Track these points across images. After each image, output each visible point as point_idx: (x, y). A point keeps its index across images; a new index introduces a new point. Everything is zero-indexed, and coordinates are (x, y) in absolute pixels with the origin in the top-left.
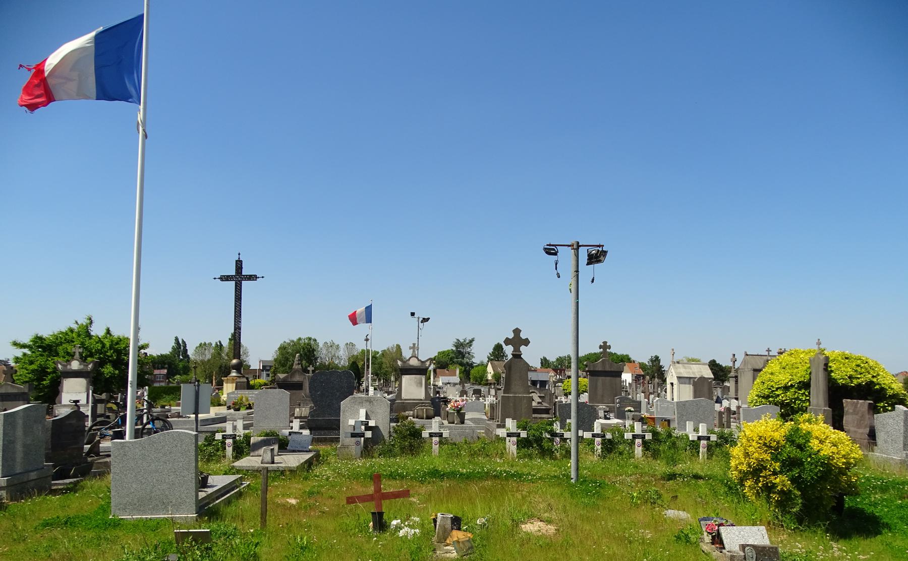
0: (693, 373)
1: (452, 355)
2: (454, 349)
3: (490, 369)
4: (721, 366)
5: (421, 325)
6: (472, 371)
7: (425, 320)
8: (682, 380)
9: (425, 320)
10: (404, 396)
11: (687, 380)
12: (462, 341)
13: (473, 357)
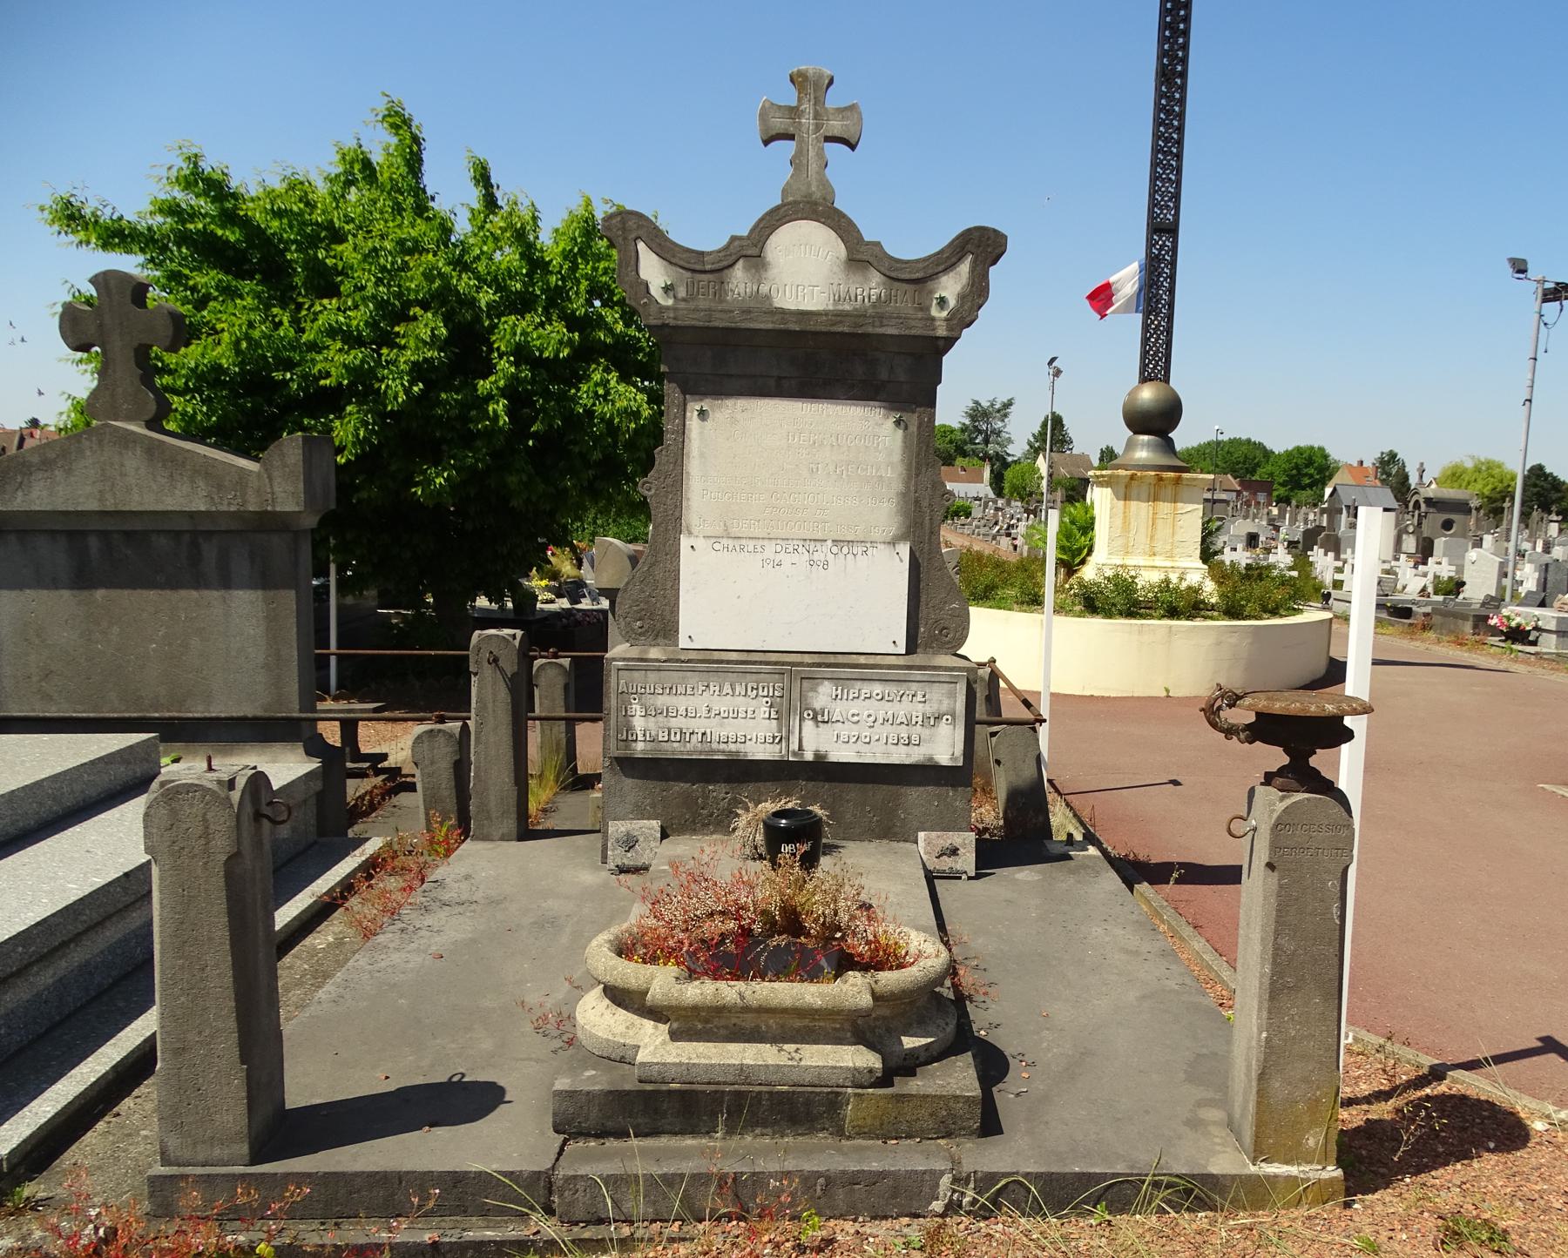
1: (959, 436)
2: (967, 422)
3: (1042, 464)
4: (1555, 478)
6: (1008, 474)
12: (985, 404)
13: (1010, 441)
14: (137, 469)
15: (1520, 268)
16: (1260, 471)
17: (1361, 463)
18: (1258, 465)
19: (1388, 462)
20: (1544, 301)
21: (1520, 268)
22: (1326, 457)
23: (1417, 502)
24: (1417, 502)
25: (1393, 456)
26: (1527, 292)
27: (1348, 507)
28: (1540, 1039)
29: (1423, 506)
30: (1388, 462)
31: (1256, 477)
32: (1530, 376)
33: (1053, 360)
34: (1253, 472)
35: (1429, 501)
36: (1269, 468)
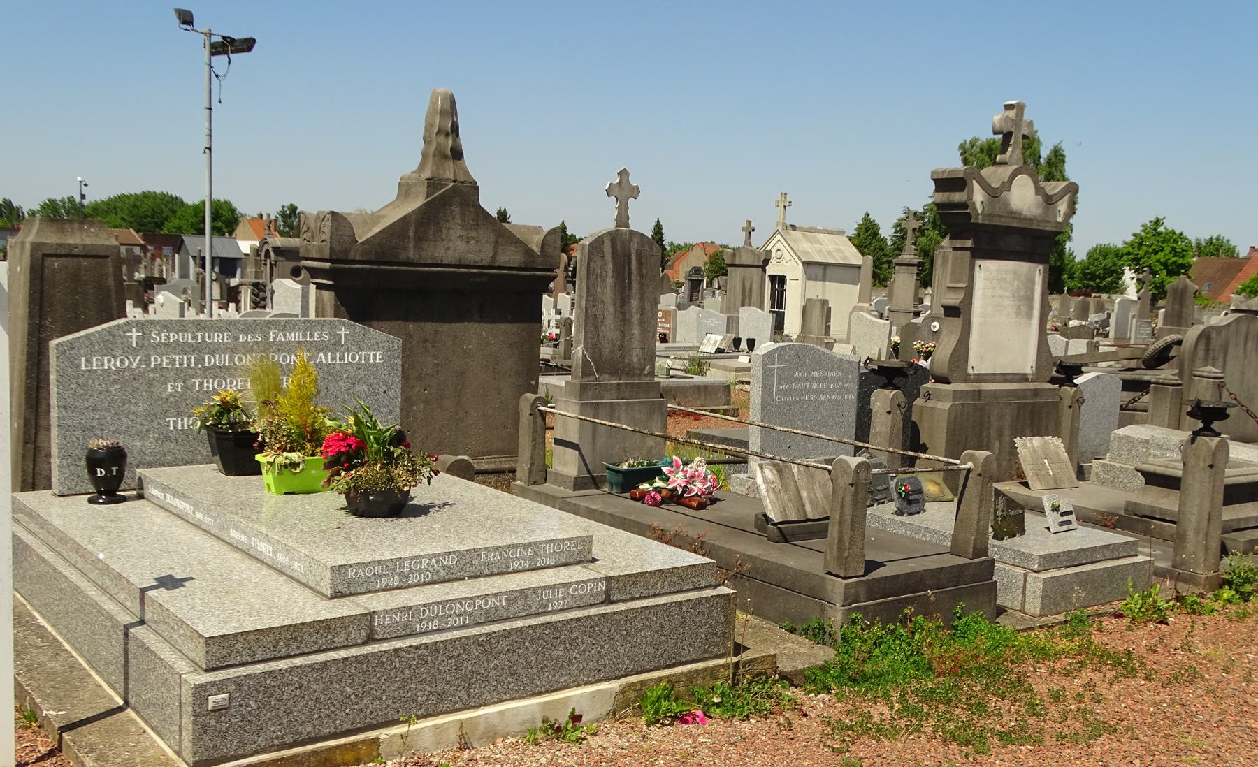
0: (829, 253)
5: (220, 61)
7: (227, 46)
8: (812, 269)
9: (227, 46)
10: (977, 362)
11: (820, 270)
14: (301, 733)
15: (186, 19)
16: (168, 225)
17: (261, 216)
18: (166, 219)
19: (290, 216)
20: (212, 54)
21: (186, 19)
22: (233, 211)
23: (267, 251)
24: (267, 251)
25: (293, 209)
26: (194, 46)
27: (194, 258)
28: (156, 579)
29: (272, 254)
30: (290, 216)
31: (165, 231)
32: (207, 125)
33: (169, 582)
34: (160, 225)
35: (276, 249)
36: (176, 222)
